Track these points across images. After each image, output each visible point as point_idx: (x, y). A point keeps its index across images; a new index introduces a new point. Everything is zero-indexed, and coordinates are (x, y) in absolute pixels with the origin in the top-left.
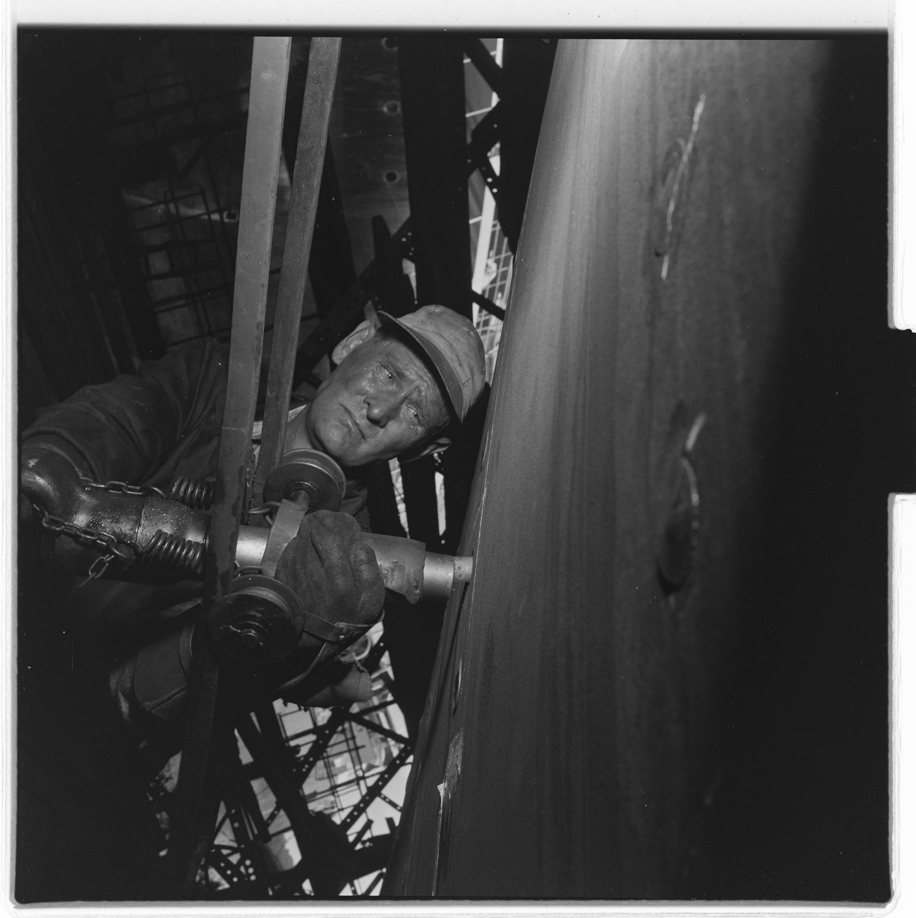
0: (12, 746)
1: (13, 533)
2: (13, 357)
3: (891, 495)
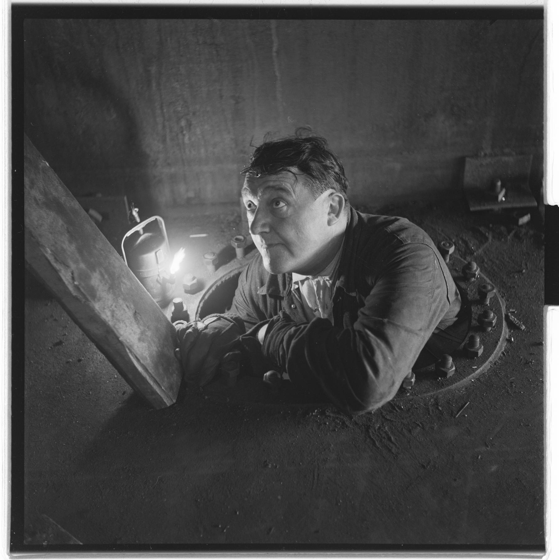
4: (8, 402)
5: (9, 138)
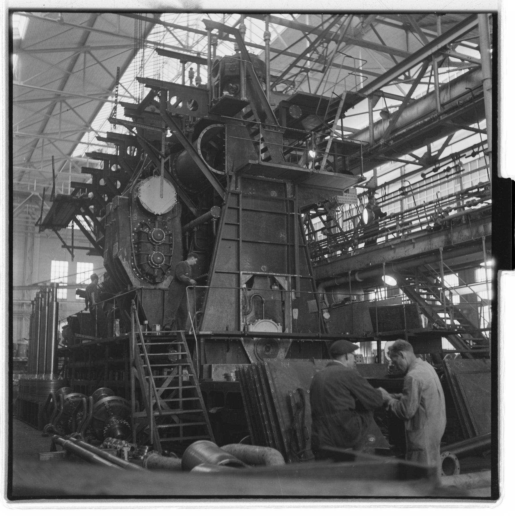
0: (6, 412)
1: (6, 293)
3: (499, 271)
4: (6, 359)
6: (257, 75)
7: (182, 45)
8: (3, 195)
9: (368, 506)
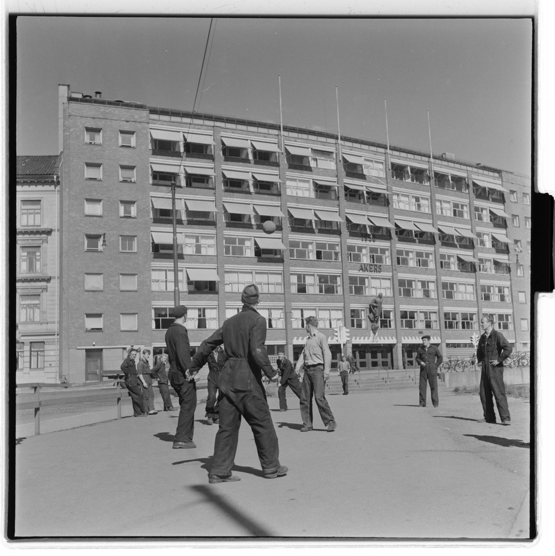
2: (6, 210)
3: (536, 293)
4: (6, 388)
5: (6, 127)
6: (284, 142)
7: (227, 442)
8: (2, 211)
9: (395, 546)
